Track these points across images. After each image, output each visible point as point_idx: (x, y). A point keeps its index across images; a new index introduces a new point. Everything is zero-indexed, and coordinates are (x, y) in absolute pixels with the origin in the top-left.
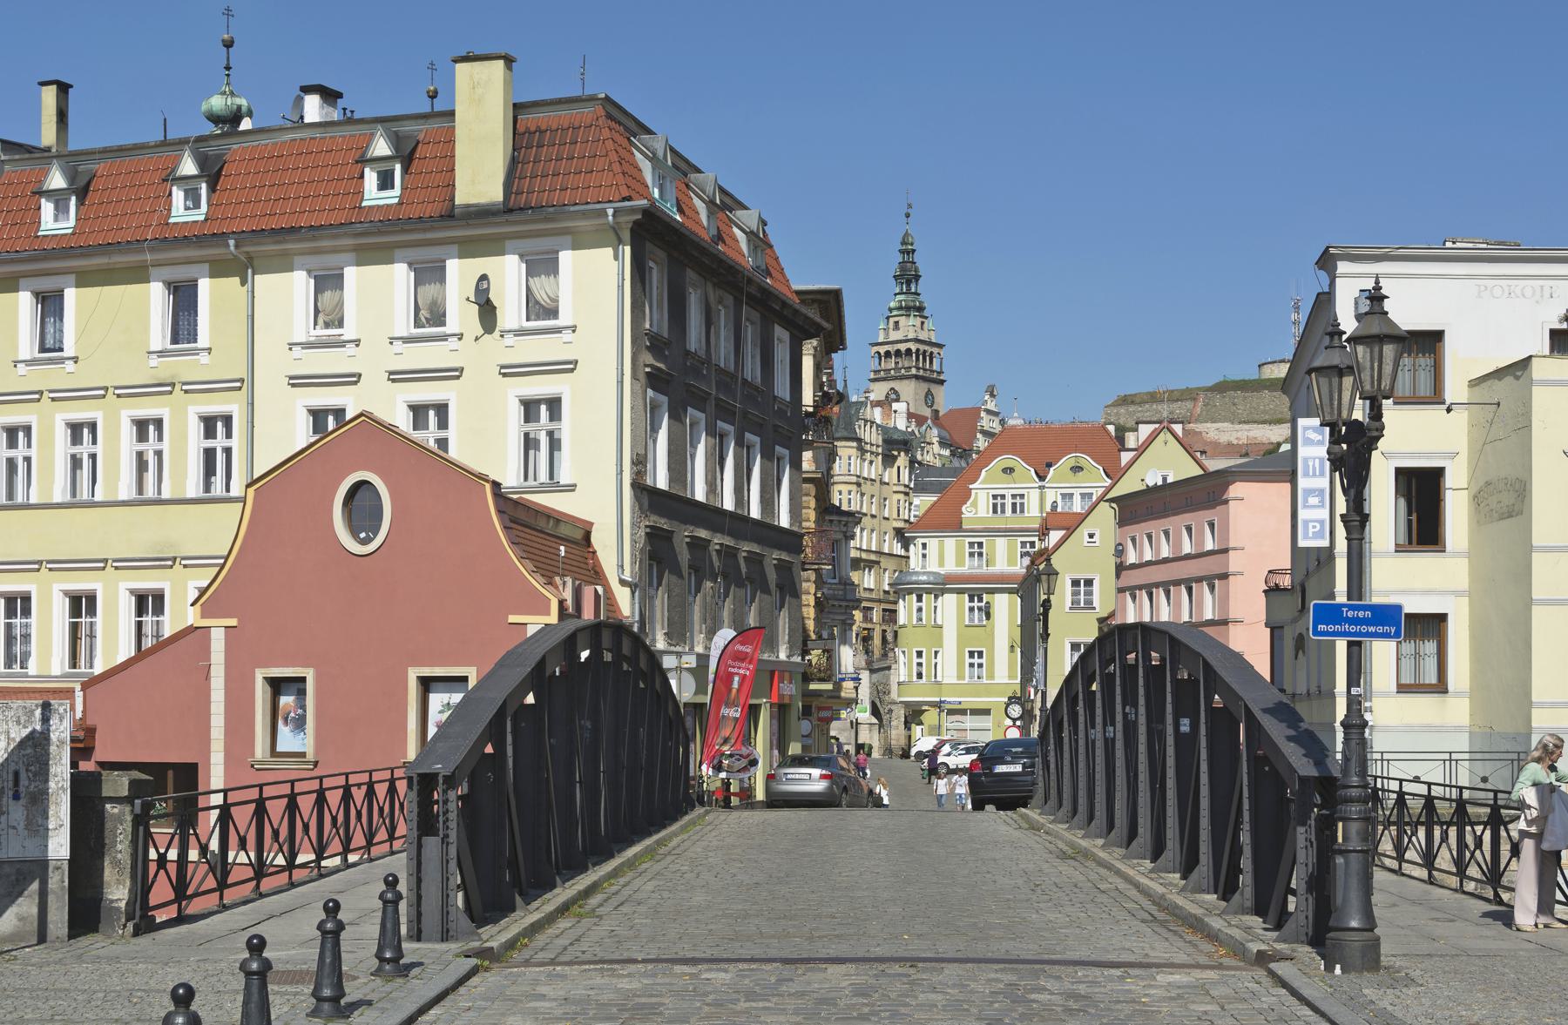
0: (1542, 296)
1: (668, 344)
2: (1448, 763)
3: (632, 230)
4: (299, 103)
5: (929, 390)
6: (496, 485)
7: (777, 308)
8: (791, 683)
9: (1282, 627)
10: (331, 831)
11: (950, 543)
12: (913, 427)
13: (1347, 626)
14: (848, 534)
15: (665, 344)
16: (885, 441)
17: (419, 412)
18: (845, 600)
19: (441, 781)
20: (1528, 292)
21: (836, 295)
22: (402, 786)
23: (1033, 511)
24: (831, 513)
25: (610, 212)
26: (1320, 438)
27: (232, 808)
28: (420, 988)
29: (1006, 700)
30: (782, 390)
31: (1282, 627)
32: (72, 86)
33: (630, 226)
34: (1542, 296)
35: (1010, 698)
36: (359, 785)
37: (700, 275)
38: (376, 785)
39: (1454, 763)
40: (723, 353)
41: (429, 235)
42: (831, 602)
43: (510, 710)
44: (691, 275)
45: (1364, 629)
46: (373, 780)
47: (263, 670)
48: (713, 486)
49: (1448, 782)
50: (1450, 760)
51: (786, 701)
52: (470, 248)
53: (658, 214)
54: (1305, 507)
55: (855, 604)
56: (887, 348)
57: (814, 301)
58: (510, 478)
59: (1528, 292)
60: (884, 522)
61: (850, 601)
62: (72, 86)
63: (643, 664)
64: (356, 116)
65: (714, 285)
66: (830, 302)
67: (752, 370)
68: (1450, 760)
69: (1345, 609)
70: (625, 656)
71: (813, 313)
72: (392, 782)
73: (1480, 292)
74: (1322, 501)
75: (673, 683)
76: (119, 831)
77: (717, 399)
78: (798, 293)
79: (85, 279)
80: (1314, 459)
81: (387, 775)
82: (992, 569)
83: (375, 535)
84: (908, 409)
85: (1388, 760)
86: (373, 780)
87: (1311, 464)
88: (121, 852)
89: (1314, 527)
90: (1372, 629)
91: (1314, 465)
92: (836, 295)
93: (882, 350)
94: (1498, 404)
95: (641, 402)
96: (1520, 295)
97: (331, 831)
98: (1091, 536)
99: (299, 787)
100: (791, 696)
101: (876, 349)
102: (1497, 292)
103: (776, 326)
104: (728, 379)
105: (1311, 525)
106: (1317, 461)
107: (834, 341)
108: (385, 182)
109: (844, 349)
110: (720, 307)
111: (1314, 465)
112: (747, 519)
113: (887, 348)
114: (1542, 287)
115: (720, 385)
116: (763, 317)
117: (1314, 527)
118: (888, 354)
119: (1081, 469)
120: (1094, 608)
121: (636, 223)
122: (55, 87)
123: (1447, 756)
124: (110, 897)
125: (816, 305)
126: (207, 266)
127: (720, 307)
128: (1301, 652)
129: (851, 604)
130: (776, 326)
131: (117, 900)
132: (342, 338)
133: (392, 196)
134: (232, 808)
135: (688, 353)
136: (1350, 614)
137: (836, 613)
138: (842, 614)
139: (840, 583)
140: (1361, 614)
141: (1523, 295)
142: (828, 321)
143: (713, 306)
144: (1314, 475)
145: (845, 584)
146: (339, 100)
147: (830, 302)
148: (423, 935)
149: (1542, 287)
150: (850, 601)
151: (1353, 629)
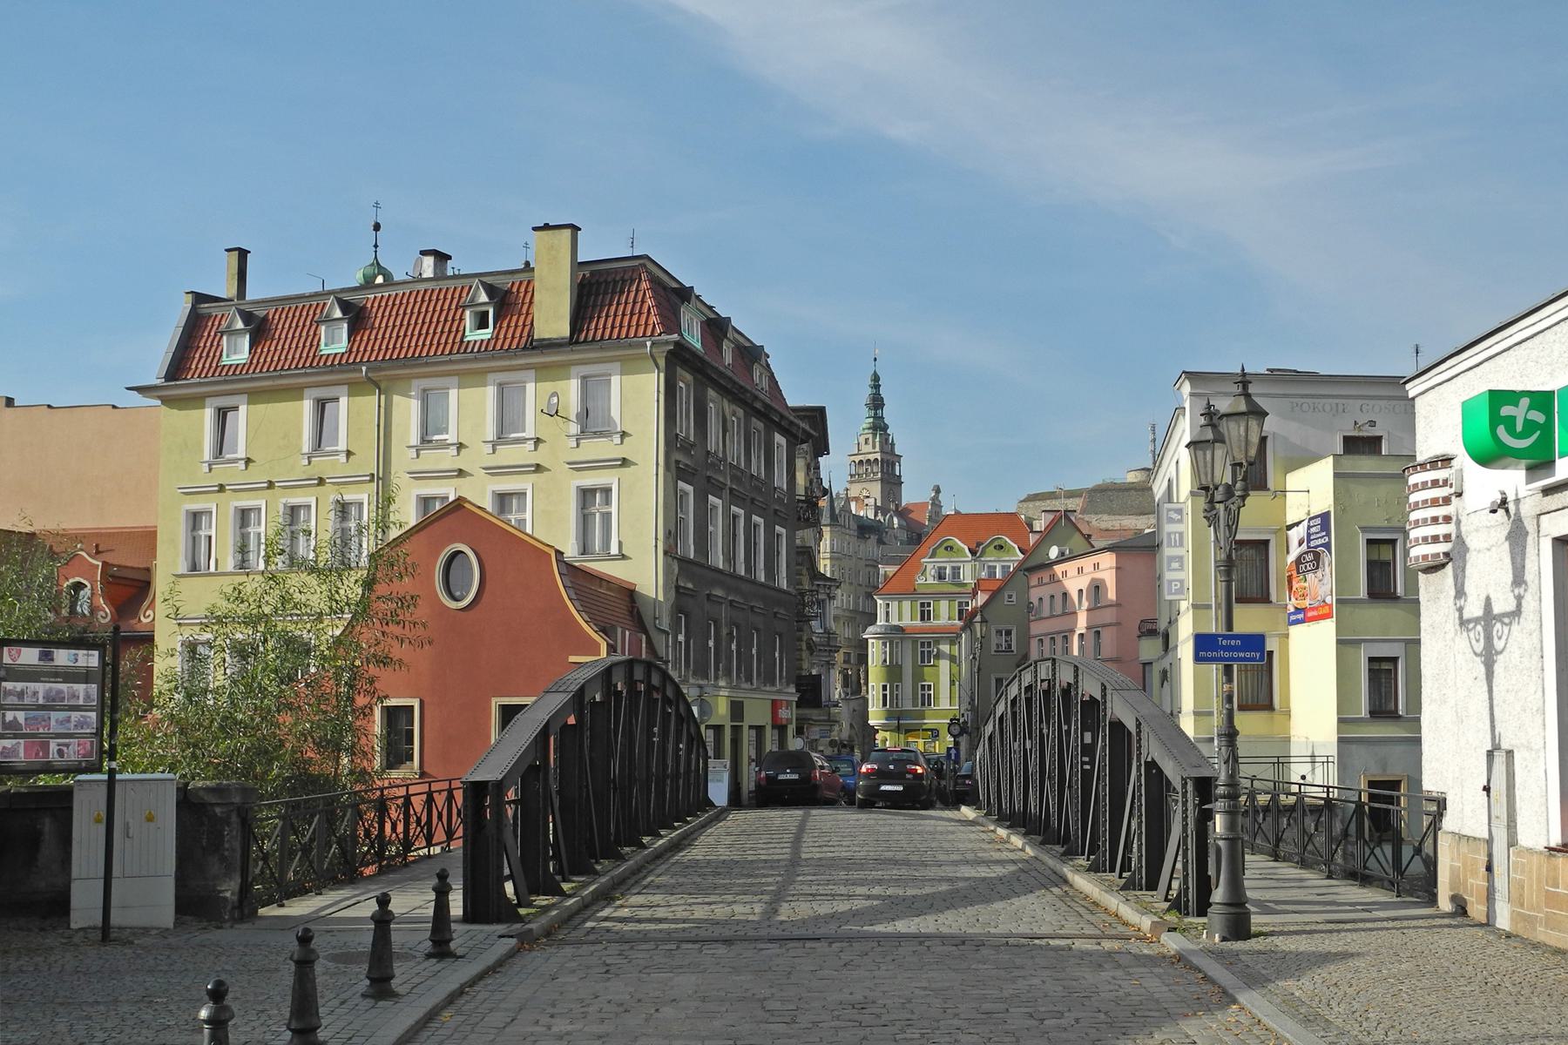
0: (1337, 411)
1: (693, 446)
2: (1325, 764)
3: (666, 358)
4: (419, 264)
5: (891, 490)
6: (559, 553)
7: (777, 420)
8: (787, 709)
9: (1151, 663)
10: (457, 820)
11: (906, 605)
12: (880, 517)
13: (1222, 652)
14: (831, 595)
15: (692, 446)
16: (858, 527)
17: (503, 499)
18: (829, 646)
19: (490, 788)
20: (1327, 408)
21: (821, 412)
22: (459, 796)
23: (967, 576)
24: (820, 579)
25: (649, 344)
26: (1179, 517)
27: (412, 798)
28: (455, 975)
29: (949, 721)
30: (780, 480)
31: (1151, 663)
32: (249, 252)
33: (665, 354)
34: (1337, 411)
35: (951, 720)
36: (440, 792)
37: (718, 393)
38: (454, 792)
39: (1281, 765)
40: (735, 453)
41: (514, 362)
42: (818, 648)
43: (556, 728)
44: (711, 393)
45: (1235, 655)
46: (410, 793)
47: (498, 699)
48: (730, 557)
49: (1326, 784)
50: (1278, 763)
51: (784, 722)
52: (544, 373)
53: (687, 345)
54: (1169, 570)
55: (837, 649)
56: (861, 458)
57: (805, 417)
58: (571, 551)
59: (1327, 408)
60: (859, 588)
61: (832, 646)
62: (249, 252)
63: (670, 693)
64: (461, 273)
65: (729, 401)
66: (817, 416)
67: (757, 467)
68: (1278, 763)
69: (1220, 639)
70: (654, 686)
71: (804, 425)
72: (450, 792)
73: (1293, 408)
74: (1182, 566)
75: (695, 709)
76: (226, 833)
77: (731, 490)
78: (795, 410)
79: (255, 396)
80: (1175, 533)
81: (445, 785)
82: (934, 622)
83: (468, 593)
84: (876, 503)
85: (1283, 763)
86: (410, 793)
87: (1173, 537)
88: (228, 850)
89: (1176, 585)
90: (1242, 655)
91: (1175, 539)
92: (821, 412)
93: (857, 459)
94: (1308, 491)
95: (672, 492)
96: (1321, 410)
97: (457, 820)
98: (1010, 597)
99: (412, 790)
100: (787, 719)
101: (852, 458)
102: (1305, 407)
103: (776, 433)
104: (738, 474)
105: (1173, 583)
106: (1177, 535)
107: (822, 447)
108: (482, 324)
109: (828, 454)
110: (734, 419)
111: (1175, 539)
112: (754, 582)
113: (861, 458)
114: (1337, 404)
115: (734, 478)
116: (766, 426)
117: (1176, 585)
118: (861, 462)
119: (1001, 547)
120: (1012, 651)
121: (670, 352)
122: (237, 252)
123: (1276, 760)
124: (219, 888)
125: (806, 420)
126: (346, 387)
127: (734, 419)
128: (1166, 682)
129: (833, 649)
130: (776, 433)
131: (223, 891)
132: (448, 442)
133: (485, 334)
134: (412, 798)
135: (708, 453)
136: (1224, 642)
137: (823, 656)
138: (826, 657)
139: (825, 632)
140: (1233, 642)
141: (1324, 410)
142: (815, 431)
143: (728, 417)
144: (1175, 546)
145: (829, 634)
146: (449, 261)
147: (817, 416)
148: (1201, 612)
149: (1337, 404)
150: (832, 646)
151: (1227, 655)
